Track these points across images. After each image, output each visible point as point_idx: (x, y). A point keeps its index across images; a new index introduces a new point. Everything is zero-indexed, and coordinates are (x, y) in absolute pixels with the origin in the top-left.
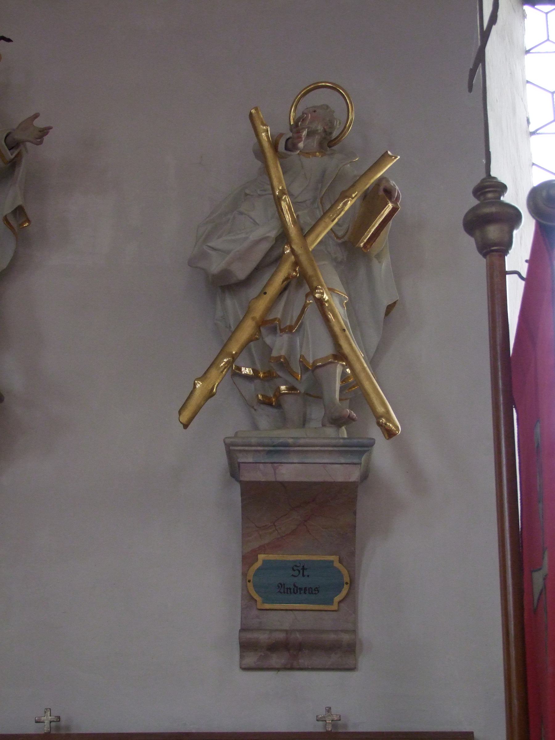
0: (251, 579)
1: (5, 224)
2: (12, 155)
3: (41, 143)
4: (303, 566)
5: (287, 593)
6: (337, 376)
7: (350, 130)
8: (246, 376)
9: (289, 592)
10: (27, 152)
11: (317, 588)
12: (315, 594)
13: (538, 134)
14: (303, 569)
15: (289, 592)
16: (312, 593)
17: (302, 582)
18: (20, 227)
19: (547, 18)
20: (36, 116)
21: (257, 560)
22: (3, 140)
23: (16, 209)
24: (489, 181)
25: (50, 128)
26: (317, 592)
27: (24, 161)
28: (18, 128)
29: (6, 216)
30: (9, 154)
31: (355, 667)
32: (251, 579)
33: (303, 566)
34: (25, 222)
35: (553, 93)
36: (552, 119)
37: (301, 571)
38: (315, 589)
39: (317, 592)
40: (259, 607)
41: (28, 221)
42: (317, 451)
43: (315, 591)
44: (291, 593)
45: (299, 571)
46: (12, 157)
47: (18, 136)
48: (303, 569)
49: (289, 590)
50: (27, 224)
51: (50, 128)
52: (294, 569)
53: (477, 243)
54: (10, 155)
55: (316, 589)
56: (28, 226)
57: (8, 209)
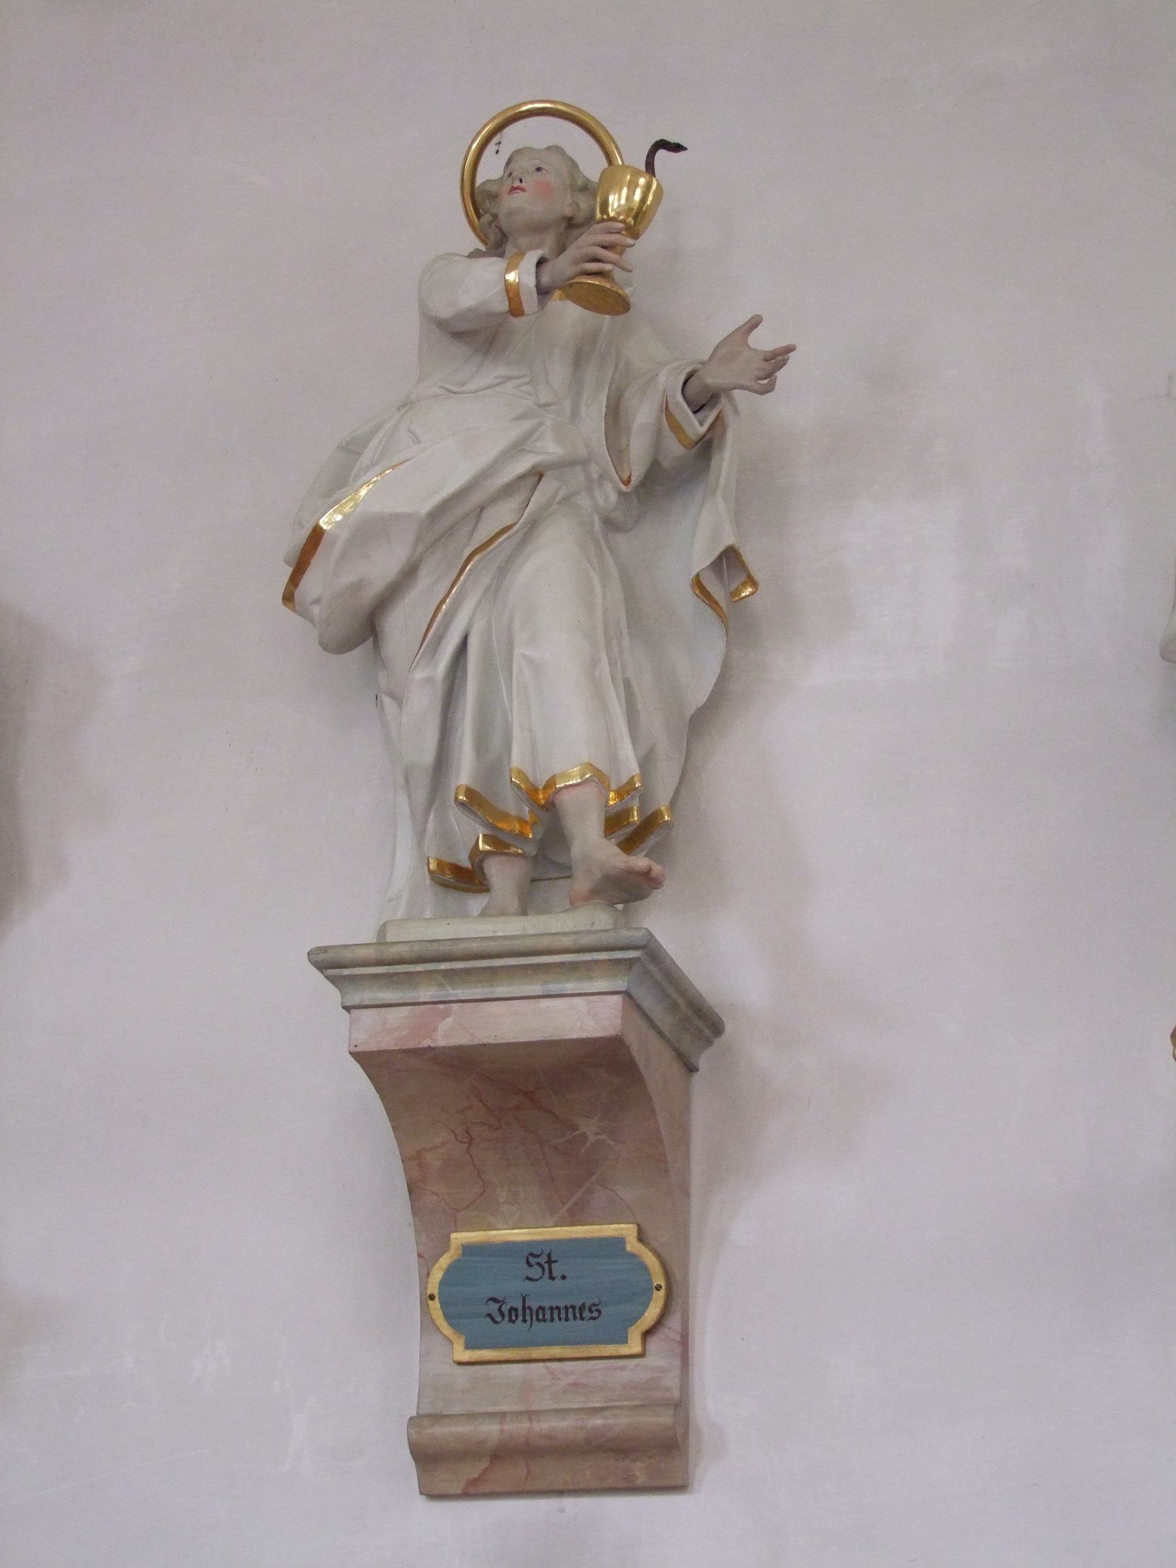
0: (436, 1292)
1: (698, 596)
2: (701, 424)
3: (769, 389)
4: (549, 1256)
5: (567, 1319)
10: (736, 412)
11: (594, 1305)
12: (593, 1318)
16: (582, 1318)
17: (545, 1293)
18: (734, 600)
20: (754, 324)
21: (445, 1246)
22: (680, 388)
23: (720, 557)
25: (790, 349)
26: (595, 1314)
27: (730, 436)
28: (711, 358)
29: (698, 575)
30: (697, 424)
32: (436, 1292)
33: (549, 1256)
34: (744, 585)
37: (546, 1266)
39: (595, 1314)
41: (753, 582)
43: (591, 1311)
46: (702, 430)
47: (713, 378)
48: (550, 1262)
49: (556, 1312)
50: (748, 591)
51: (790, 349)
52: (531, 1262)
54: (696, 427)
55: (594, 1309)
56: (752, 594)
57: (701, 559)
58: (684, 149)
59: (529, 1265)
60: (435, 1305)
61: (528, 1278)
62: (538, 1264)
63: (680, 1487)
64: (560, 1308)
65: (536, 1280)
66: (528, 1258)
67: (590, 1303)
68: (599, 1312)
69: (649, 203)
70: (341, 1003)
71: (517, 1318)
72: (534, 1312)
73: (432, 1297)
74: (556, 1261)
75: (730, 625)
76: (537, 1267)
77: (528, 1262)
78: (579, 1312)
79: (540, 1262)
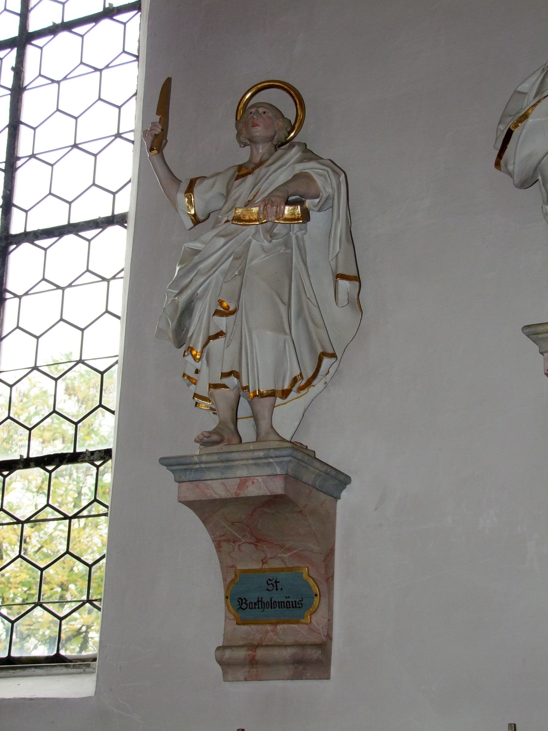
4: (276, 580)
6: (293, 280)
9: (294, 603)
11: (300, 601)
12: (299, 607)
14: (276, 582)
15: (294, 603)
16: (296, 607)
24: (212, 399)
26: (300, 606)
31: (327, 582)
33: (276, 580)
37: (275, 584)
38: (298, 602)
40: (340, 306)
42: (290, 314)
43: (298, 604)
44: (284, 607)
45: (273, 585)
53: (97, 219)
59: (269, 584)
60: (229, 600)
61: (267, 589)
68: (301, 604)
70: (539, 351)
72: (248, 604)
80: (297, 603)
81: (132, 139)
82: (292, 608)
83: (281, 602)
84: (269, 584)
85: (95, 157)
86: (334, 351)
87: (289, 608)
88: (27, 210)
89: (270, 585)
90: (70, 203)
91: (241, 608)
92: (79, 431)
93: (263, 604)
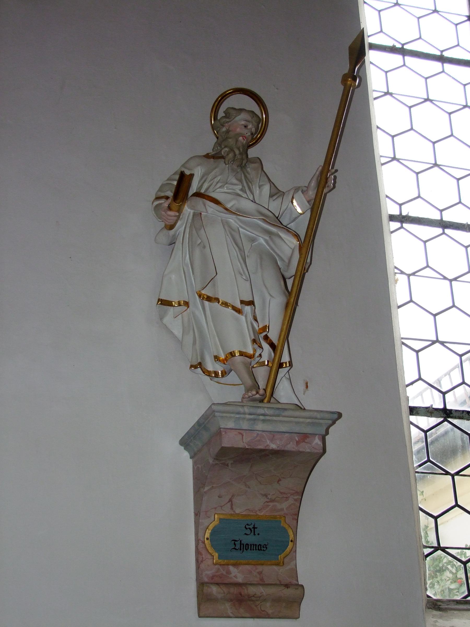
4: (254, 525)
7: (316, 223)
8: (220, 377)
11: (265, 545)
12: (264, 550)
13: (433, 103)
14: (254, 528)
16: (261, 550)
17: (250, 539)
19: (462, 47)
26: (265, 549)
33: (254, 525)
35: (466, 247)
36: (467, 270)
37: (253, 530)
38: (263, 546)
39: (265, 549)
43: (264, 547)
44: (256, 550)
49: (255, 546)
58: (340, 415)
59: (246, 529)
61: (246, 534)
62: (249, 528)
63: (296, 617)
64: (249, 545)
65: (249, 535)
66: (246, 526)
67: (258, 544)
68: (266, 548)
69: (254, 137)
71: (248, 548)
73: (292, 541)
74: (256, 528)
75: (190, 221)
76: (249, 529)
77: (245, 527)
78: (260, 548)
79: (250, 527)
80: (262, 546)
81: (381, 158)
82: (255, 550)
83: (253, 545)
84: (246, 529)
85: (444, 234)
86: (286, 373)
87: (260, 551)
88: (411, 108)
89: (248, 529)
90: (419, 197)
91: (234, 548)
92: (468, 443)
93: (242, 546)
